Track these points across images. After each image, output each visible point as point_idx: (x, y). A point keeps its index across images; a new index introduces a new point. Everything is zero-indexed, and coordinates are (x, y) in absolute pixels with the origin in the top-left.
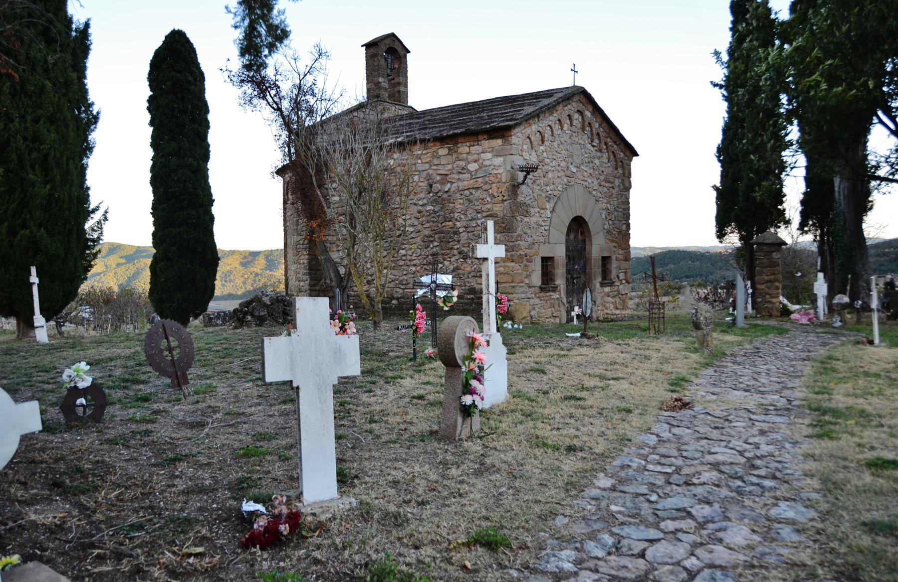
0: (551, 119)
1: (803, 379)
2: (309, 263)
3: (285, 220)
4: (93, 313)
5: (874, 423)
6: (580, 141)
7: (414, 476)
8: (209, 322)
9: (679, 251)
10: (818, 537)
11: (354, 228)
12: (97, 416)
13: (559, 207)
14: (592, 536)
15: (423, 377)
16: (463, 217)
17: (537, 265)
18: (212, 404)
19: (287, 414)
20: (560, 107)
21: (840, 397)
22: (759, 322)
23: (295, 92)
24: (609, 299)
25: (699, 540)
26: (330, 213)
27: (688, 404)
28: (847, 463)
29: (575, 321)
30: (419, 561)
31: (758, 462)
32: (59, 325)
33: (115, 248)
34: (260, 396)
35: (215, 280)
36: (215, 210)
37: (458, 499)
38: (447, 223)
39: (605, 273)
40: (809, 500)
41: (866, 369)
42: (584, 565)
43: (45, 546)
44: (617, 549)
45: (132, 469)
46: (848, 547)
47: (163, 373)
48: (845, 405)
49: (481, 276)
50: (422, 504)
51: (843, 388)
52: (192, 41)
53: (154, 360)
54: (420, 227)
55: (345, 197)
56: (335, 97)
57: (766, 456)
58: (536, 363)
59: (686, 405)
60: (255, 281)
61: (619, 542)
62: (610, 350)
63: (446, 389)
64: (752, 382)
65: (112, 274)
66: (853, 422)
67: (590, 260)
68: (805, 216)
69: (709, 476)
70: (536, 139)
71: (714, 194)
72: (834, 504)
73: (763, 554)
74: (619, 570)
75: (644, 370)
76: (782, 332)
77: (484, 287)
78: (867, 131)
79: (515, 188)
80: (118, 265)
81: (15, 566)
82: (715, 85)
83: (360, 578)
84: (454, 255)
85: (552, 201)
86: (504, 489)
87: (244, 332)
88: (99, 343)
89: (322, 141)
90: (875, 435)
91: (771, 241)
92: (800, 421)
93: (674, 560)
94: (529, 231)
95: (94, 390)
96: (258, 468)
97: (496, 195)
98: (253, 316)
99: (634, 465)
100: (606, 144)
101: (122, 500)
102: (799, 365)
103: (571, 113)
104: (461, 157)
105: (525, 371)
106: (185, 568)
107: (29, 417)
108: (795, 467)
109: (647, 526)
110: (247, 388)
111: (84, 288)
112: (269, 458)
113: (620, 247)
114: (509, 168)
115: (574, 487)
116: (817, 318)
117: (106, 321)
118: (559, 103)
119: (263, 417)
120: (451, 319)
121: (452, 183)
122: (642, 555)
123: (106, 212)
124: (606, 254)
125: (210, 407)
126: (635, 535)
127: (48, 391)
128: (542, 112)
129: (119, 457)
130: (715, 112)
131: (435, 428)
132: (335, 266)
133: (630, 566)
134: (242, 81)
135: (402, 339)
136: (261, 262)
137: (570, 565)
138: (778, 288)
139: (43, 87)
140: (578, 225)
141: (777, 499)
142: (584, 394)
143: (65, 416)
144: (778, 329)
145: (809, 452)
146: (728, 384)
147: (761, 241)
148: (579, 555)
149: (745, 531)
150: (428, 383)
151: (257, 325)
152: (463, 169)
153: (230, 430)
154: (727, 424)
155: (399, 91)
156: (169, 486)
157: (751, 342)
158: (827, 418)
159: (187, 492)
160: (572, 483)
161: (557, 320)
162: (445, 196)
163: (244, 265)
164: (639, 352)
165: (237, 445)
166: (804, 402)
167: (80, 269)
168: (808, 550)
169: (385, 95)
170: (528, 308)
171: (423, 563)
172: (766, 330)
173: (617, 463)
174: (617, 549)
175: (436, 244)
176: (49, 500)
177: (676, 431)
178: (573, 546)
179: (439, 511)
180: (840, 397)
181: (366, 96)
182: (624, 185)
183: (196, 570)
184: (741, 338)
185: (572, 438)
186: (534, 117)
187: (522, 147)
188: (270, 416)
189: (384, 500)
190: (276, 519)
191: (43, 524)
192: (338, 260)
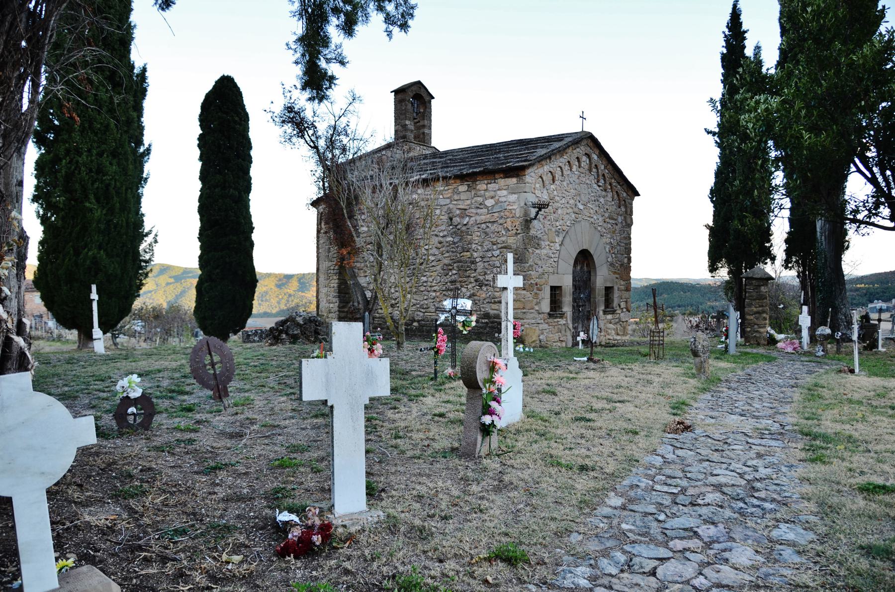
0: (562, 161)
1: (793, 405)
2: (339, 287)
3: (318, 247)
4: (144, 327)
5: (861, 449)
6: (588, 181)
7: (437, 491)
8: (247, 338)
9: (672, 282)
10: (818, 559)
11: (381, 256)
12: (146, 425)
13: (567, 240)
14: (606, 553)
15: (443, 396)
17: (546, 294)
18: (249, 416)
19: (319, 428)
20: (570, 150)
21: (828, 423)
22: (748, 350)
23: (331, 132)
24: (611, 326)
25: (706, 560)
26: (359, 242)
27: (690, 427)
28: (840, 487)
29: (581, 346)
30: (444, 575)
31: (758, 485)
32: (114, 337)
33: (165, 269)
34: (294, 410)
35: (253, 300)
36: (254, 237)
37: (479, 515)
38: (465, 253)
39: (608, 302)
40: (807, 522)
41: (849, 396)
42: (598, 582)
43: (98, 546)
44: (629, 567)
45: (176, 475)
46: (848, 570)
47: (204, 384)
48: (834, 431)
49: (500, 302)
50: (445, 518)
51: (829, 415)
52: (239, 85)
53: (198, 373)
55: (373, 227)
56: (367, 136)
57: (764, 479)
58: (548, 385)
59: (687, 428)
60: (288, 301)
61: (631, 560)
62: (615, 374)
63: (467, 409)
64: (747, 407)
65: (161, 292)
66: (842, 447)
67: (594, 289)
68: (789, 253)
69: (713, 497)
70: (547, 178)
71: (708, 232)
72: (831, 527)
73: (767, 575)
74: (631, 587)
75: (648, 393)
76: (770, 360)
77: (503, 315)
78: (845, 178)
79: (527, 222)
80: (168, 284)
81: (72, 568)
82: (709, 133)
83: (388, 589)
86: (522, 506)
87: (278, 349)
88: (149, 355)
89: (352, 177)
90: (864, 460)
91: (759, 276)
92: (794, 445)
93: (684, 579)
94: (539, 262)
95: (145, 401)
96: (292, 479)
97: (510, 228)
98: (287, 334)
99: (643, 485)
100: (610, 184)
101: (167, 505)
102: (789, 391)
104: (479, 193)
105: (538, 393)
106: (224, 574)
107: (84, 431)
108: (794, 491)
109: (656, 545)
110: (282, 402)
111: (137, 304)
112: (302, 469)
113: (621, 278)
114: (522, 204)
115: (587, 505)
116: (802, 347)
117: (156, 334)
118: (569, 147)
119: (297, 431)
120: (474, 344)
122: (653, 573)
123: (156, 235)
124: (609, 285)
125: (248, 419)
126: (646, 553)
127: (103, 399)
128: (553, 154)
129: (163, 463)
130: (708, 157)
131: (456, 445)
132: (362, 290)
133: (642, 584)
134: (283, 122)
135: (423, 359)
136: (295, 284)
137: (586, 581)
138: (765, 319)
139: (107, 126)
140: (584, 258)
141: (778, 521)
142: (592, 416)
143: (118, 424)
144: (766, 357)
145: (805, 475)
146: (725, 409)
147: (750, 275)
148: (593, 572)
149: (750, 552)
150: (448, 402)
151: (290, 343)
152: (481, 204)
153: (266, 441)
154: (726, 446)
155: (424, 133)
156: (210, 493)
157: (743, 369)
158: (818, 442)
159: (227, 500)
160: (585, 501)
161: (564, 344)
162: (464, 228)
163: (279, 286)
164: (641, 376)
165: (272, 456)
166: (795, 428)
167: (134, 288)
168: (810, 572)
169: (411, 136)
170: (538, 332)
171: (448, 576)
172: (756, 358)
173: (626, 482)
174: (629, 567)
175: (454, 272)
176: (101, 502)
177: (679, 452)
178: (587, 563)
179: (461, 526)
180: (828, 423)
181: (393, 137)
183: (234, 576)
184: (734, 365)
185: (583, 458)
187: (535, 185)
188: (303, 429)
189: (410, 514)
190: (309, 530)
191: (96, 526)
192: (365, 285)
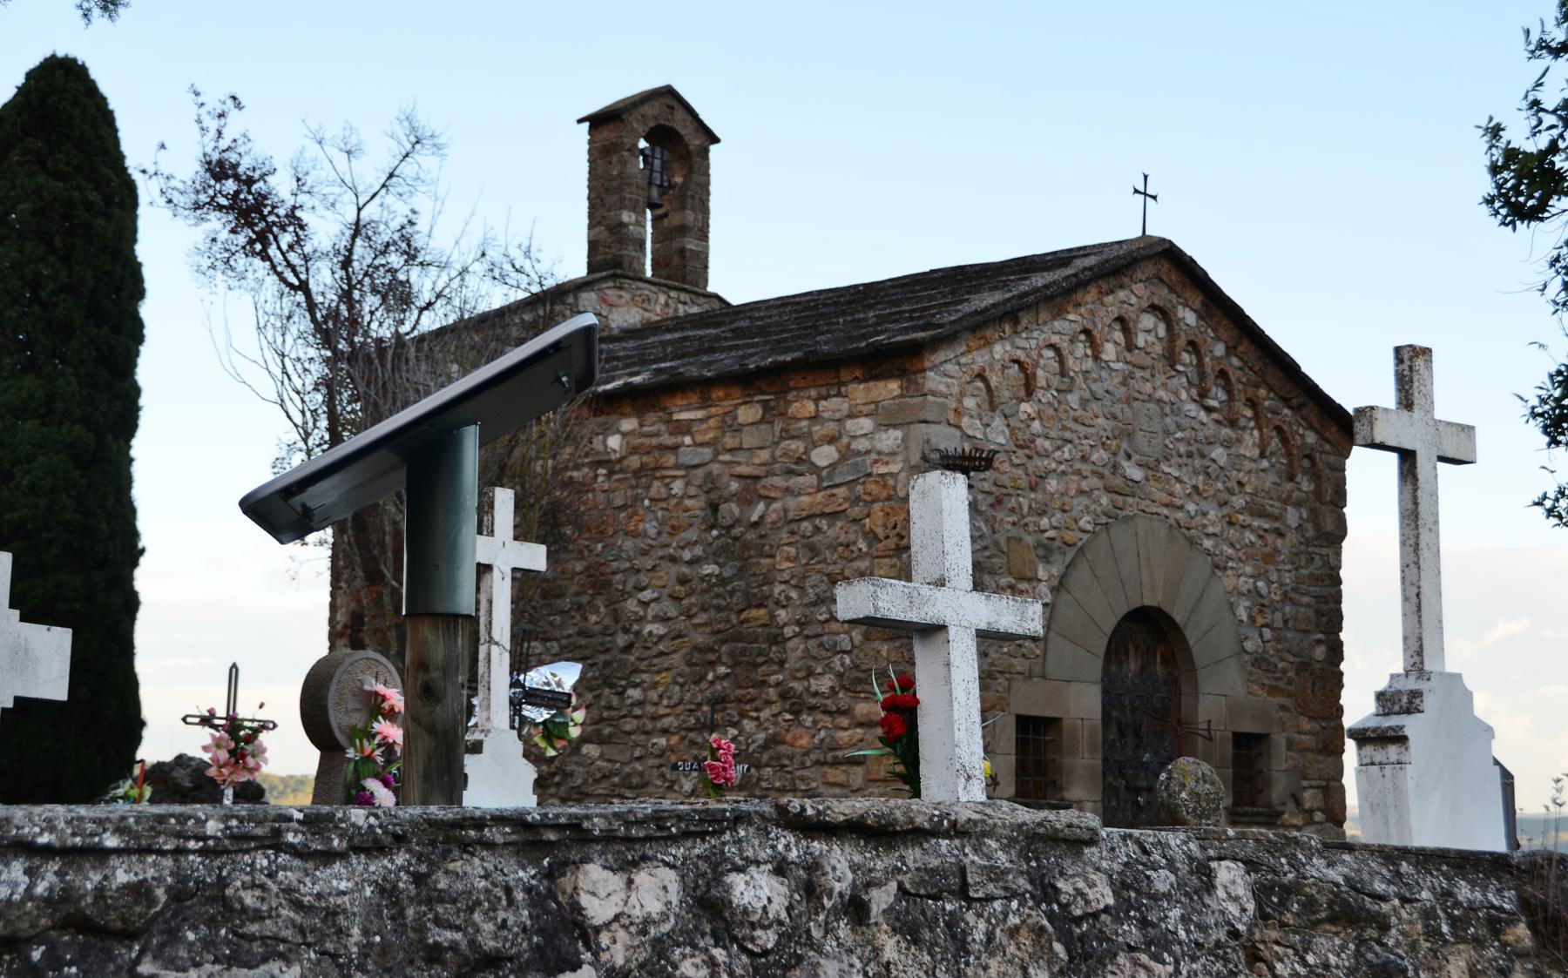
6: (1161, 394)
13: (1082, 573)
16: (794, 594)
20: (1091, 295)
38: (754, 613)
52: (104, 87)
54: (681, 624)
70: (1005, 382)
84: (769, 703)
85: (1056, 557)
97: (880, 532)
100: (1252, 403)
103: (1130, 313)
113: (1303, 710)
121: (769, 500)
124: (1248, 727)
128: (1028, 307)
152: (799, 461)
155: (682, 251)
162: (751, 536)
175: (722, 670)
182: (1317, 527)
186: (1001, 319)
